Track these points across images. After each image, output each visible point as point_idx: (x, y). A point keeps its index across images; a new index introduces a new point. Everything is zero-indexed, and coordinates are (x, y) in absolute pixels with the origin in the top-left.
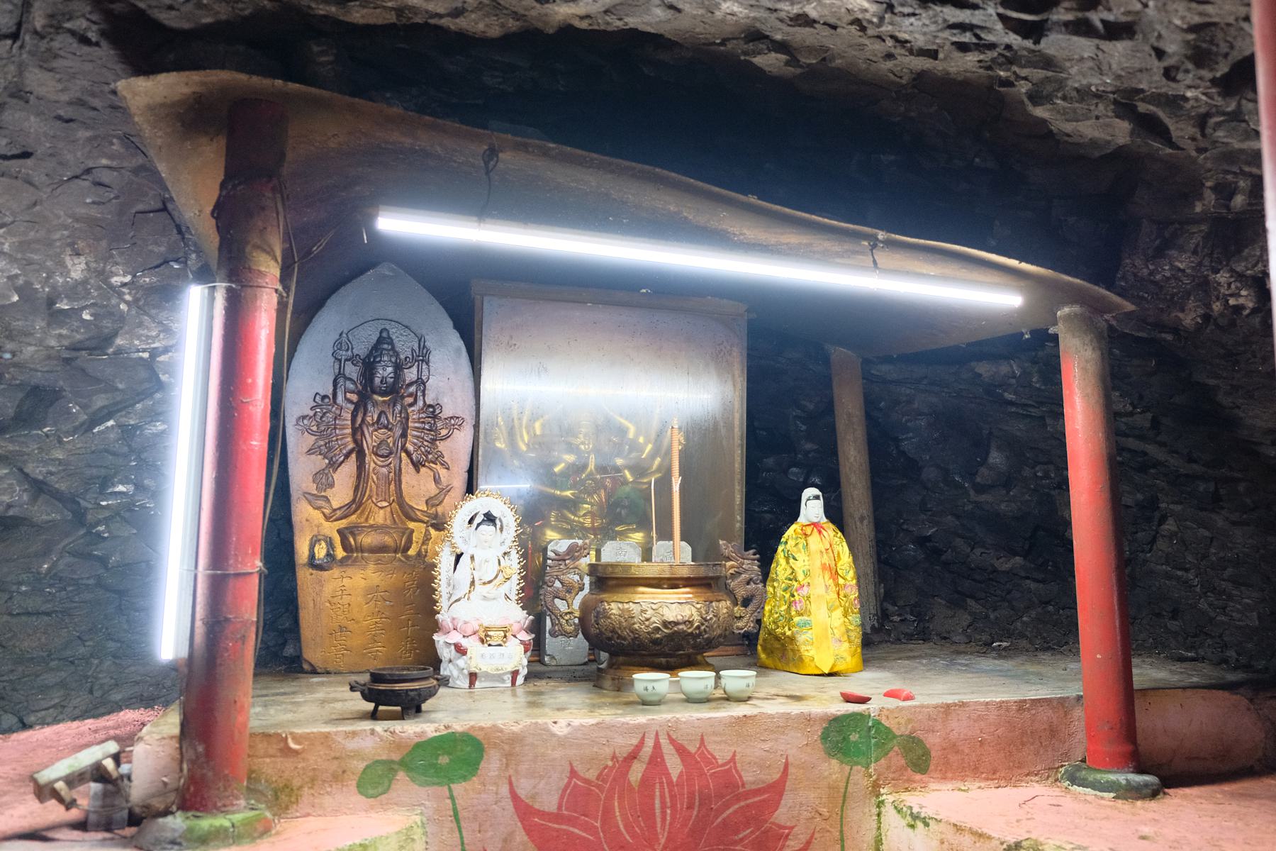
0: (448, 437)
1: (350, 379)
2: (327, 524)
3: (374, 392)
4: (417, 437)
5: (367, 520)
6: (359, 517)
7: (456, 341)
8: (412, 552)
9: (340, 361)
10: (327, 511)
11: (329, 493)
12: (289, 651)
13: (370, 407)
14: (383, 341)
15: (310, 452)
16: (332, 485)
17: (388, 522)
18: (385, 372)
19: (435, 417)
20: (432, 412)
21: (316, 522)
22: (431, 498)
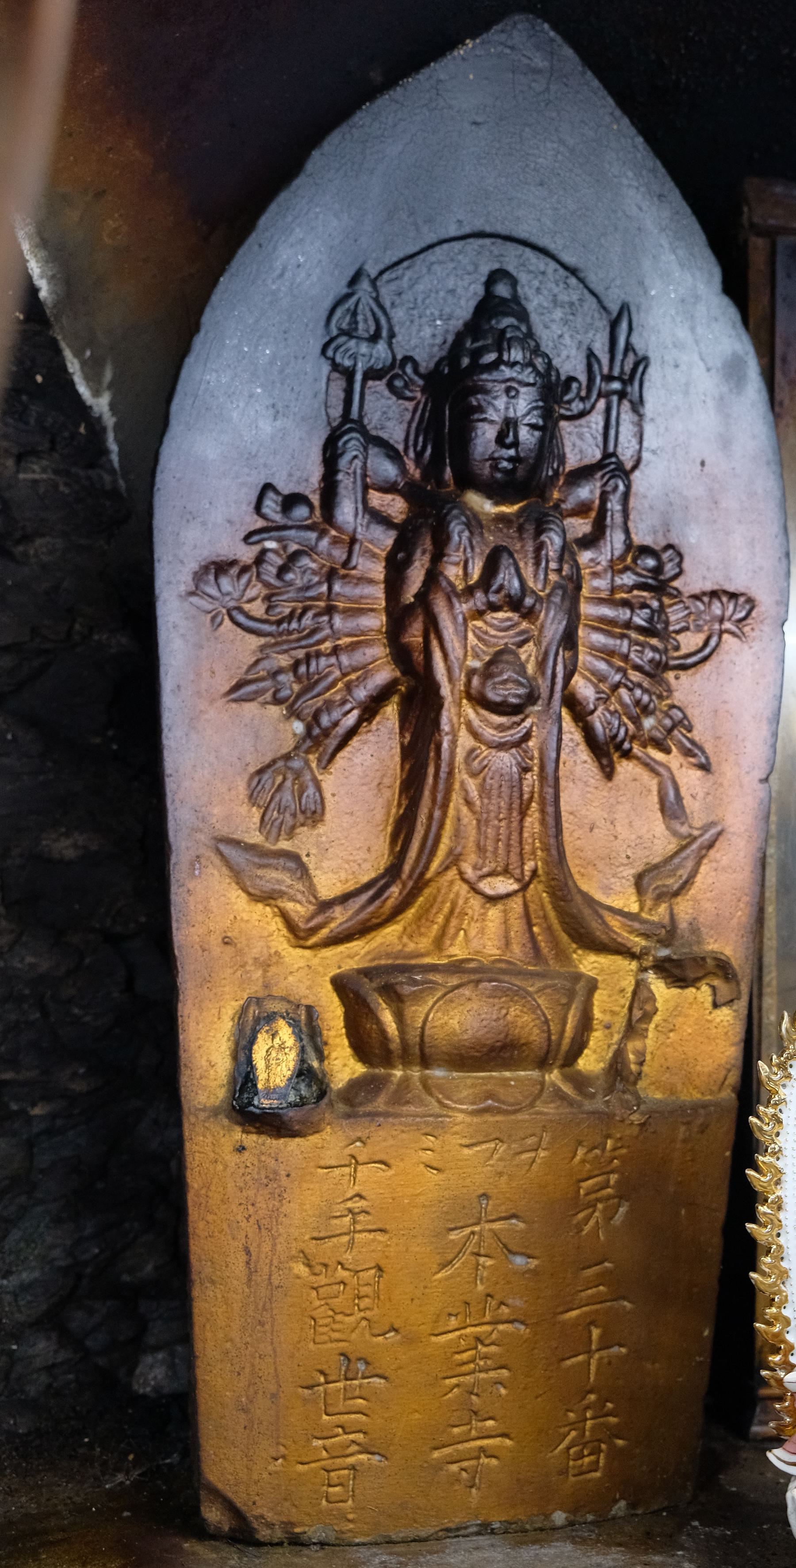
0: (703, 657)
2: (296, 957)
3: (467, 480)
4: (608, 654)
5: (439, 943)
6: (410, 933)
8: (590, 1062)
9: (349, 375)
10: (298, 910)
11: (305, 842)
12: (152, 1374)
13: (457, 530)
14: (495, 316)
15: (239, 690)
16: (314, 815)
17: (517, 951)
18: (508, 404)
19: (659, 585)
20: (656, 571)
21: (257, 950)
22: (652, 869)
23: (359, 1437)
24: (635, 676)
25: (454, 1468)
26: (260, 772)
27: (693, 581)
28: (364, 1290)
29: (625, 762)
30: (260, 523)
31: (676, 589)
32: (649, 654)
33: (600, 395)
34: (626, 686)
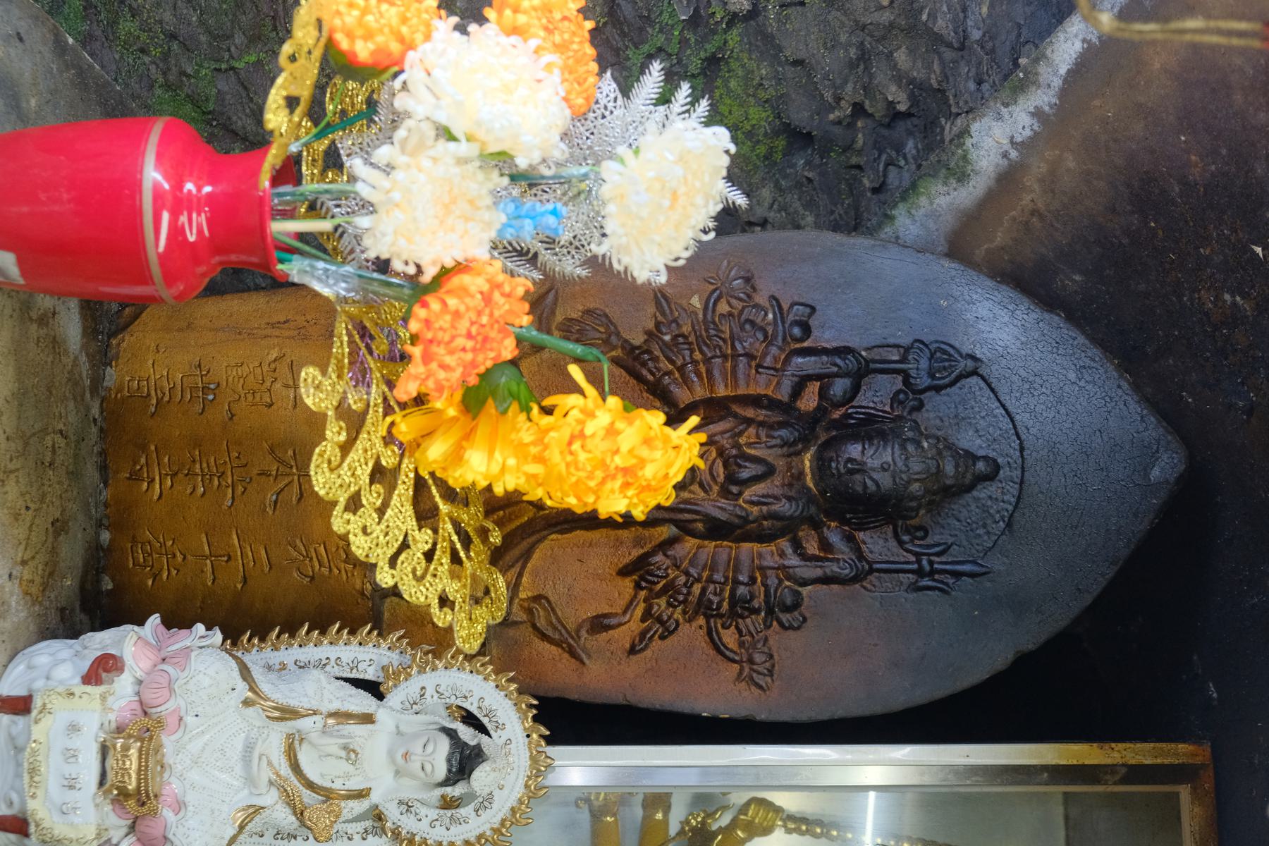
0: (718, 647)
1: (856, 389)
7: (985, 657)
23: (166, 398)
24: (697, 589)
25: (143, 461)
26: (606, 316)
27: (776, 637)
28: (258, 396)
29: (632, 585)
30: (785, 307)
31: (771, 625)
32: (716, 600)
33: (916, 554)
34: (687, 581)
